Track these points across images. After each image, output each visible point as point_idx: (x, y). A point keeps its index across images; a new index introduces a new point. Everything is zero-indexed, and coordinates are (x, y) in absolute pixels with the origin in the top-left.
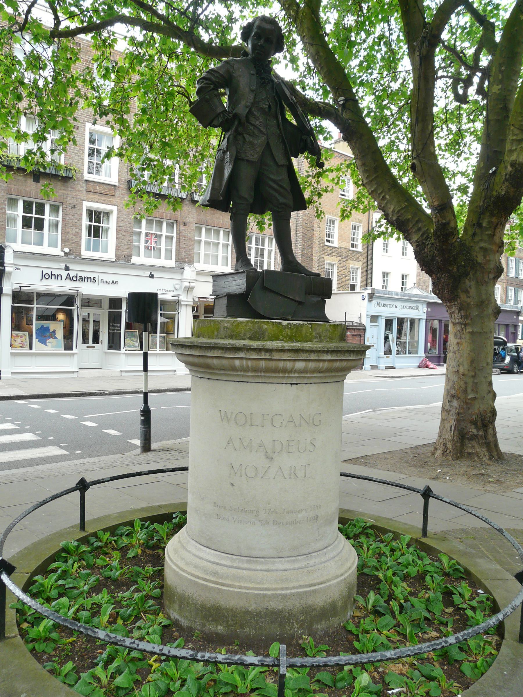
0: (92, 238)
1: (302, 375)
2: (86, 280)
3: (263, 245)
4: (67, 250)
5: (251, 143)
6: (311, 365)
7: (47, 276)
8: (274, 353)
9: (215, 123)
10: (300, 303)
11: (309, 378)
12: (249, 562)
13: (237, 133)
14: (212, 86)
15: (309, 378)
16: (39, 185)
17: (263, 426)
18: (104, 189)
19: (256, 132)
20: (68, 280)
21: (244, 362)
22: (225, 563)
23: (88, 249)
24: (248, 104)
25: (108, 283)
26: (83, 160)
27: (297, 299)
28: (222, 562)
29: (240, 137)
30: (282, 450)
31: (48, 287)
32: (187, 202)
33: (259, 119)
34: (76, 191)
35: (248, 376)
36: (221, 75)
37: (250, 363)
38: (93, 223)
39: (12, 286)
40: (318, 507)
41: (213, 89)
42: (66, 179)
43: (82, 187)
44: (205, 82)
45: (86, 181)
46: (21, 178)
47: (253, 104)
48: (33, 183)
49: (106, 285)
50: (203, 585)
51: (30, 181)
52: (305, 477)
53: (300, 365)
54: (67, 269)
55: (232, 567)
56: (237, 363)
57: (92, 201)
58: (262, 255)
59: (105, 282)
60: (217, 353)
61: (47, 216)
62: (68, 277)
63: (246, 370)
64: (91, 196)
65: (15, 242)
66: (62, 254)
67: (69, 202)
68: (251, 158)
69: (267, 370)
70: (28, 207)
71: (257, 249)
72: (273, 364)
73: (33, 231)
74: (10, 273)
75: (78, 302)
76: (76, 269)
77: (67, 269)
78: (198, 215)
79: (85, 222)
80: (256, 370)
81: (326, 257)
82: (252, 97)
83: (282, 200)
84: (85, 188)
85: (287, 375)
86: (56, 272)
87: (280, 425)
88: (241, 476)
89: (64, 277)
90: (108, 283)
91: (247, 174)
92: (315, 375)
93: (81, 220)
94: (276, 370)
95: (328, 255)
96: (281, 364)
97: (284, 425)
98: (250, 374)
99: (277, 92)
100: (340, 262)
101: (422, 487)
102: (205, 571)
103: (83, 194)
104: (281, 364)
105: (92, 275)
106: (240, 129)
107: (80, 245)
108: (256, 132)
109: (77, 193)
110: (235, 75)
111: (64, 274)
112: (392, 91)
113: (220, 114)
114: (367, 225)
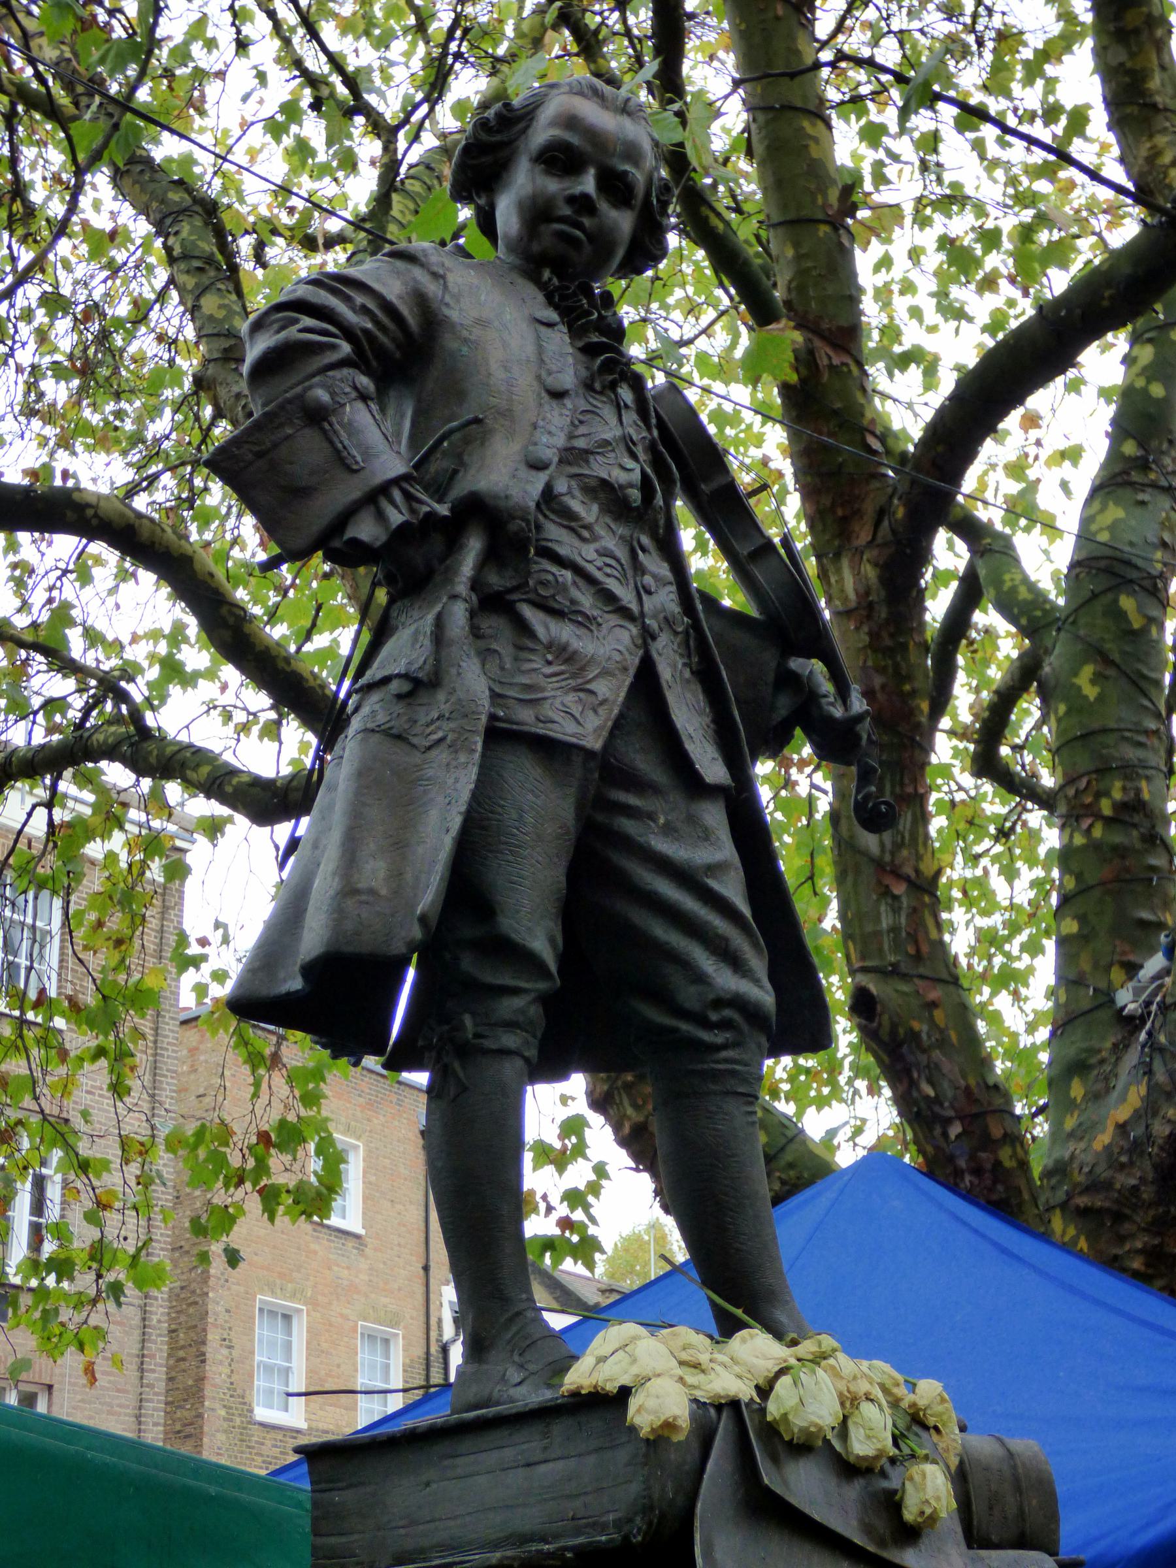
5: (563, 654)
19: (586, 600)
33: (595, 538)
36: (389, 308)
68: (565, 730)
83: (726, 980)
99: (661, 425)
110: (454, 315)
112: (125, 453)
114: (421, 1334)
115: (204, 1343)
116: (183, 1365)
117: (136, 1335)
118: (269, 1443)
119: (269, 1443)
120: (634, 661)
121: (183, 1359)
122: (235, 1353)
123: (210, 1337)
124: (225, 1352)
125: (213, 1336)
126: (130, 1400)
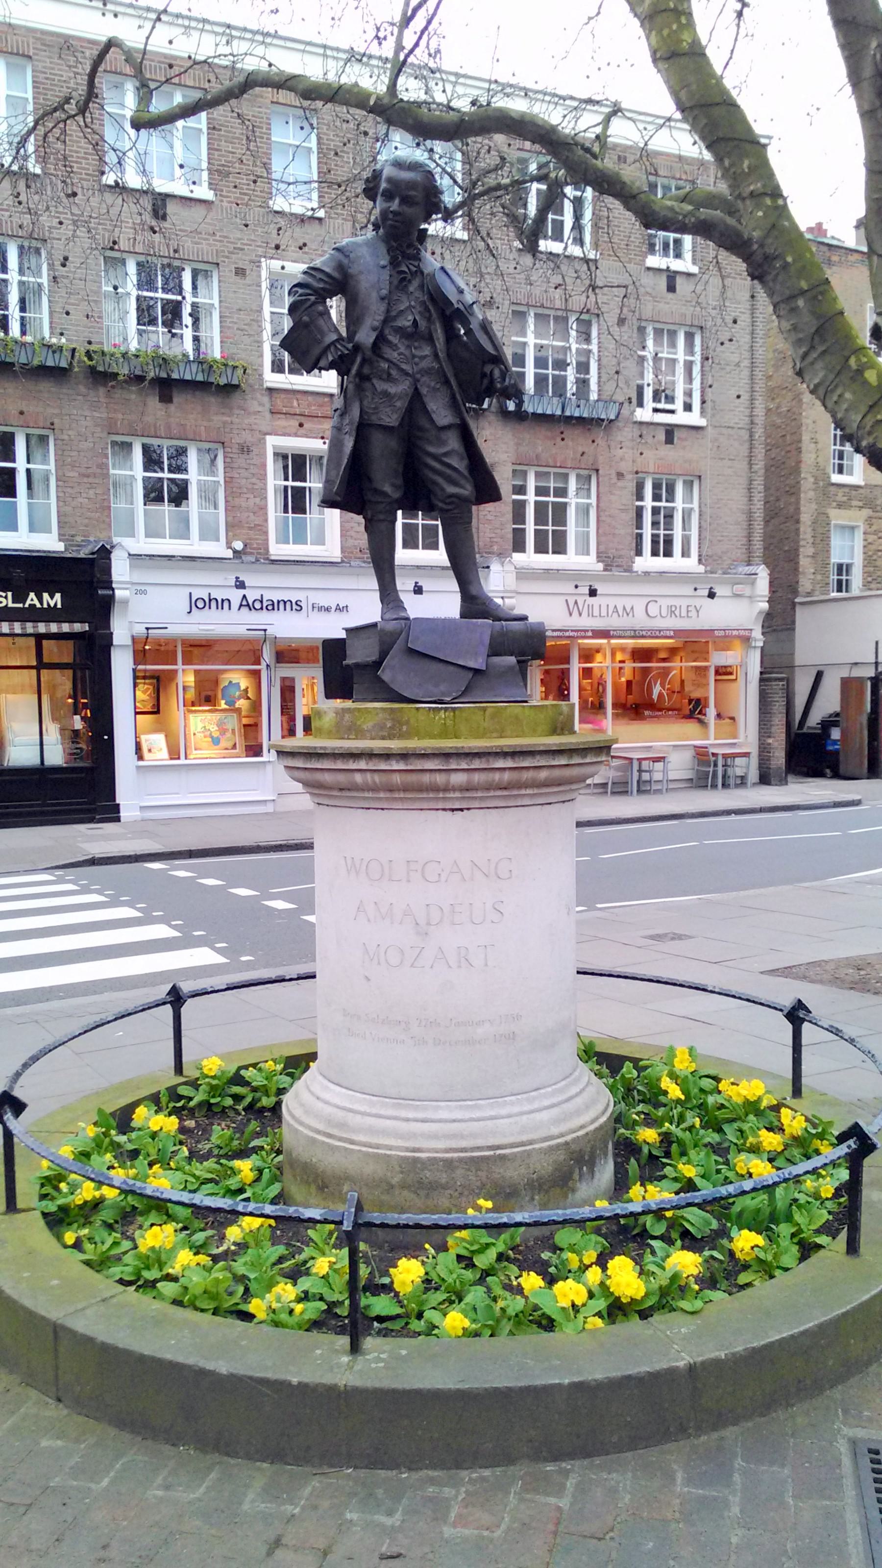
0: (290, 515)
1: (468, 794)
2: (282, 605)
3: (671, 498)
4: (238, 545)
5: (386, 394)
6: (477, 777)
7: (200, 604)
8: (411, 760)
9: (322, 363)
10: (477, 672)
11: (481, 798)
12: (395, 1106)
13: (363, 378)
14: (313, 298)
15: (481, 798)
16: (172, 408)
17: (409, 881)
18: (309, 405)
20: (245, 610)
21: (369, 776)
22: (362, 1108)
23: (283, 539)
24: (376, 324)
25: (328, 609)
26: (260, 343)
27: (471, 664)
28: (356, 1107)
29: (367, 385)
30: (441, 921)
31: (202, 627)
32: (492, 417)
34: (249, 414)
35: (380, 799)
37: (377, 778)
38: (290, 483)
39: (130, 629)
40: (518, 1017)
41: (314, 304)
42: (230, 389)
43: (261, 404)
44: (300, 291)
45: (270, 390)
46: (133, 396)
47: (385, 321)
48: (159, 405)
49: (323, 614)
50: (323, 1142)
51: (153, 403)
52: (486, 965)
53: (458, 779)
54: (240, 585)
55: (370, 1115)
56: (358, 778)
57: (284, 435)
58: (669, 525)
59: (320, 609)
60: (362, 765)
61: (194, 475)
62: (245, 604)
63: (374, 789)
64: (282, 422)
65: (132, 534)
66: (229, 554)
67: (237, 440)
69: (406, 789)
70: (151, 461)
71: (655, 511)
72: (412, 778)
73: (166, 508)
74: (125, 602)
75: (267, 655)
76: (261, 583)
77: (240, 585)
78: (518, 445)
79: (274, 481)
80: (390, 789)
81: (833, 513)
82: (383, 307)
83: (451, 489)
84: (268, 406)
85: (441, 795)
86: (219, 594)
87: (437, 879)
88: (379, 963)
89: (235, 604)
90: (328, 609)
91: (382, 448)
92: (492, 793)
93: (263, 478)
94: (421, 788)
95: (840, 506)
96: (426, 778)
97: (443, 878)
98: (382, 795)
100: (869, 521)
101: (787, 1002)
102: (329, 1122)
103: (264, 421)
104: (426, 778)
105: (294, 596)
106: (366, 370)
107: (266, 533)
108: (394, 372)
109: (251, 420)
111: (236, 596)
113: (329, 346)
115: (800, 441)
116: (789, 455)
117: (747, 445)
118: (840, 494)
119: (840, 494)
120: (410, 391)
121: (789, 451)
122: (819, 446)
123: (804, 438)
124: (813, 445)
125: (806, 438)
126: (744, 481)
